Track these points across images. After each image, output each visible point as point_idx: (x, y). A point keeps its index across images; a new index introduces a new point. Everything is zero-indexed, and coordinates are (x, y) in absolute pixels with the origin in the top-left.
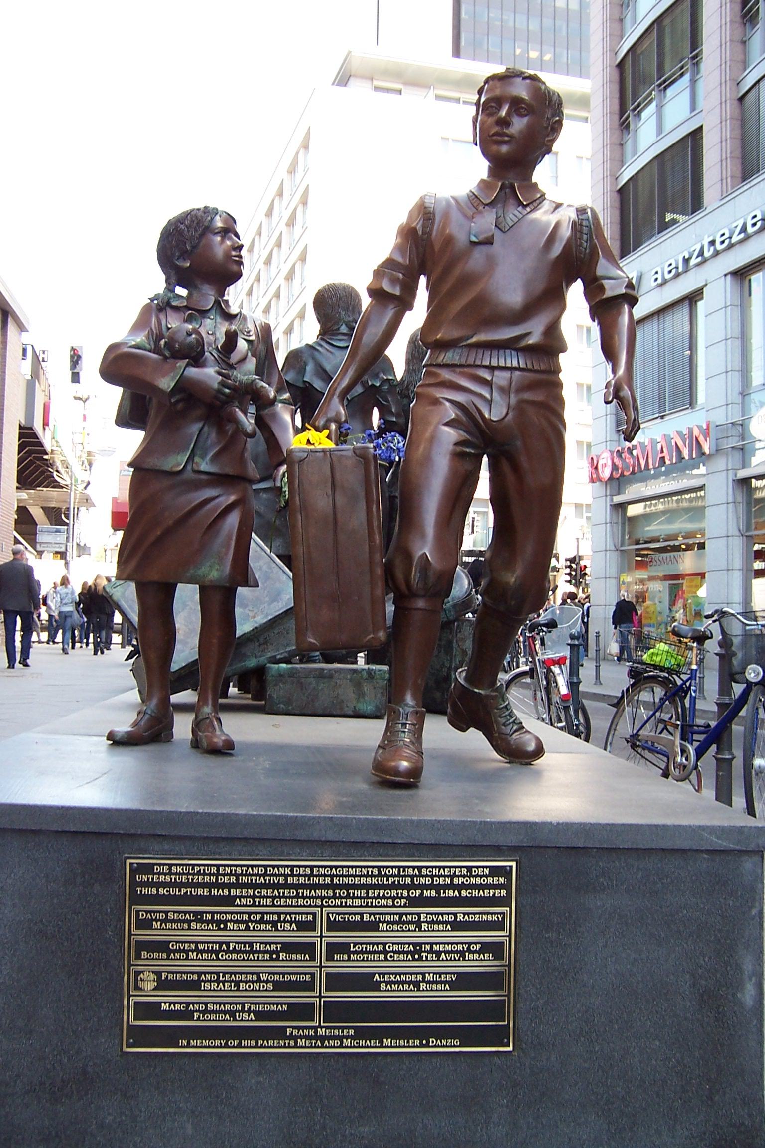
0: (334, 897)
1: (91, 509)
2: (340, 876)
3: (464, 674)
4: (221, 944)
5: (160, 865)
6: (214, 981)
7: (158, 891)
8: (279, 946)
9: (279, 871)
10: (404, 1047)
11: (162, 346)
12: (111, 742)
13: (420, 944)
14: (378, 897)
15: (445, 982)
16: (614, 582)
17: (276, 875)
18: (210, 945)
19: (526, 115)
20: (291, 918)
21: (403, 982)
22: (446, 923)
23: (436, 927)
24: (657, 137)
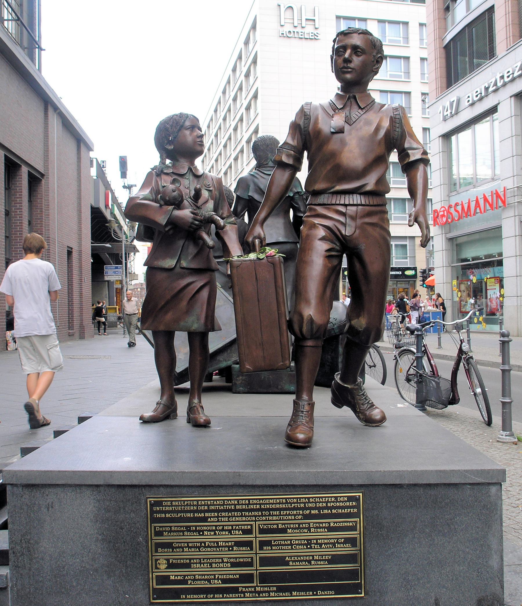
0: (262, 516)
1: (137, 254)
2: (265, 504)
3: (339, 376)
4: (201, 543)
5: (166, 501)
6: (198, 563)
7: (165, 515)
8: (233, 543)
9: (231, 502)
10: (304, 596)
11: (159, 199)
12: (142, 421)
13: (311, 540)
14: (286, 515)
15: (325, 560)
16: (449, 285)
17: (230, 505)
18: (195, 544)
19: (361, 55)
20: (239, 528)
21: (302, 561)
22: (325, 528)
23: (319, 530)
24: (467, 13)
